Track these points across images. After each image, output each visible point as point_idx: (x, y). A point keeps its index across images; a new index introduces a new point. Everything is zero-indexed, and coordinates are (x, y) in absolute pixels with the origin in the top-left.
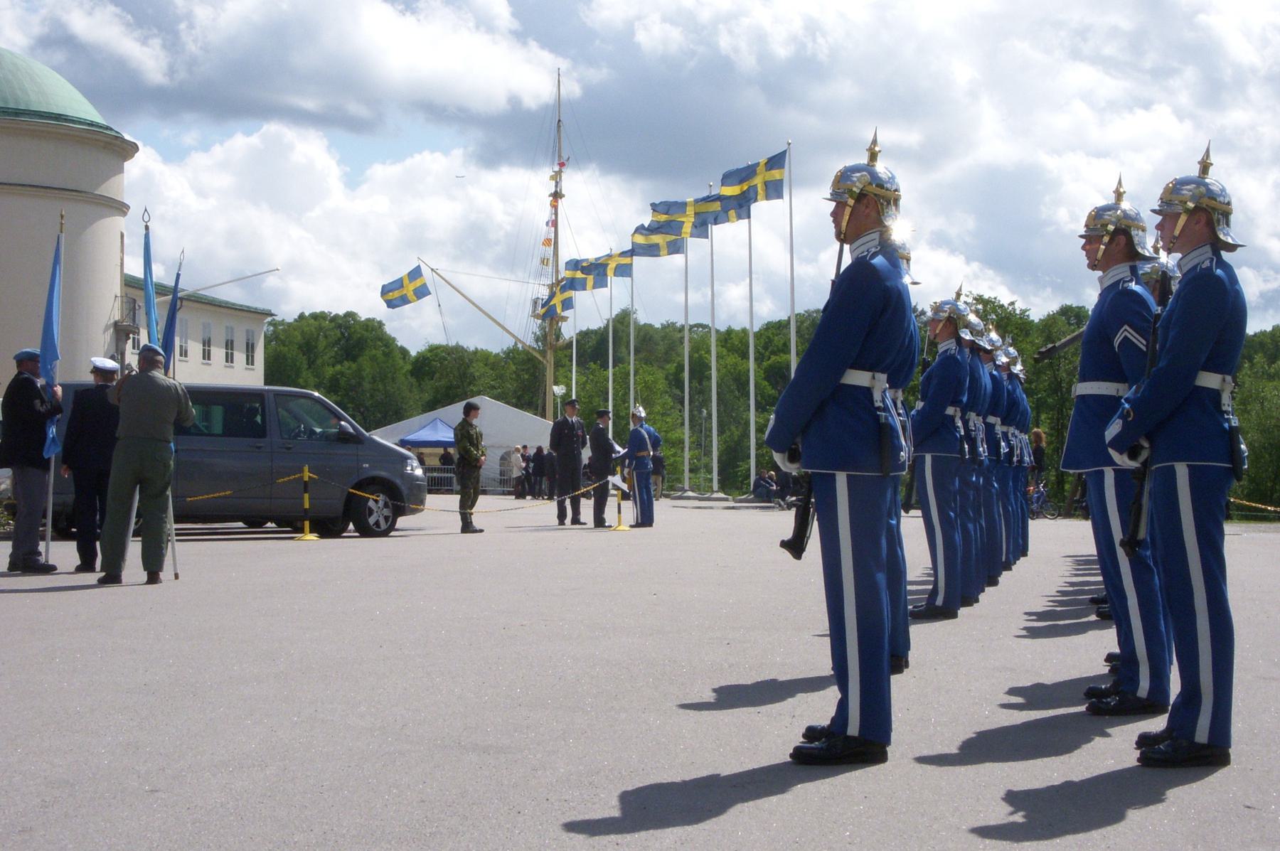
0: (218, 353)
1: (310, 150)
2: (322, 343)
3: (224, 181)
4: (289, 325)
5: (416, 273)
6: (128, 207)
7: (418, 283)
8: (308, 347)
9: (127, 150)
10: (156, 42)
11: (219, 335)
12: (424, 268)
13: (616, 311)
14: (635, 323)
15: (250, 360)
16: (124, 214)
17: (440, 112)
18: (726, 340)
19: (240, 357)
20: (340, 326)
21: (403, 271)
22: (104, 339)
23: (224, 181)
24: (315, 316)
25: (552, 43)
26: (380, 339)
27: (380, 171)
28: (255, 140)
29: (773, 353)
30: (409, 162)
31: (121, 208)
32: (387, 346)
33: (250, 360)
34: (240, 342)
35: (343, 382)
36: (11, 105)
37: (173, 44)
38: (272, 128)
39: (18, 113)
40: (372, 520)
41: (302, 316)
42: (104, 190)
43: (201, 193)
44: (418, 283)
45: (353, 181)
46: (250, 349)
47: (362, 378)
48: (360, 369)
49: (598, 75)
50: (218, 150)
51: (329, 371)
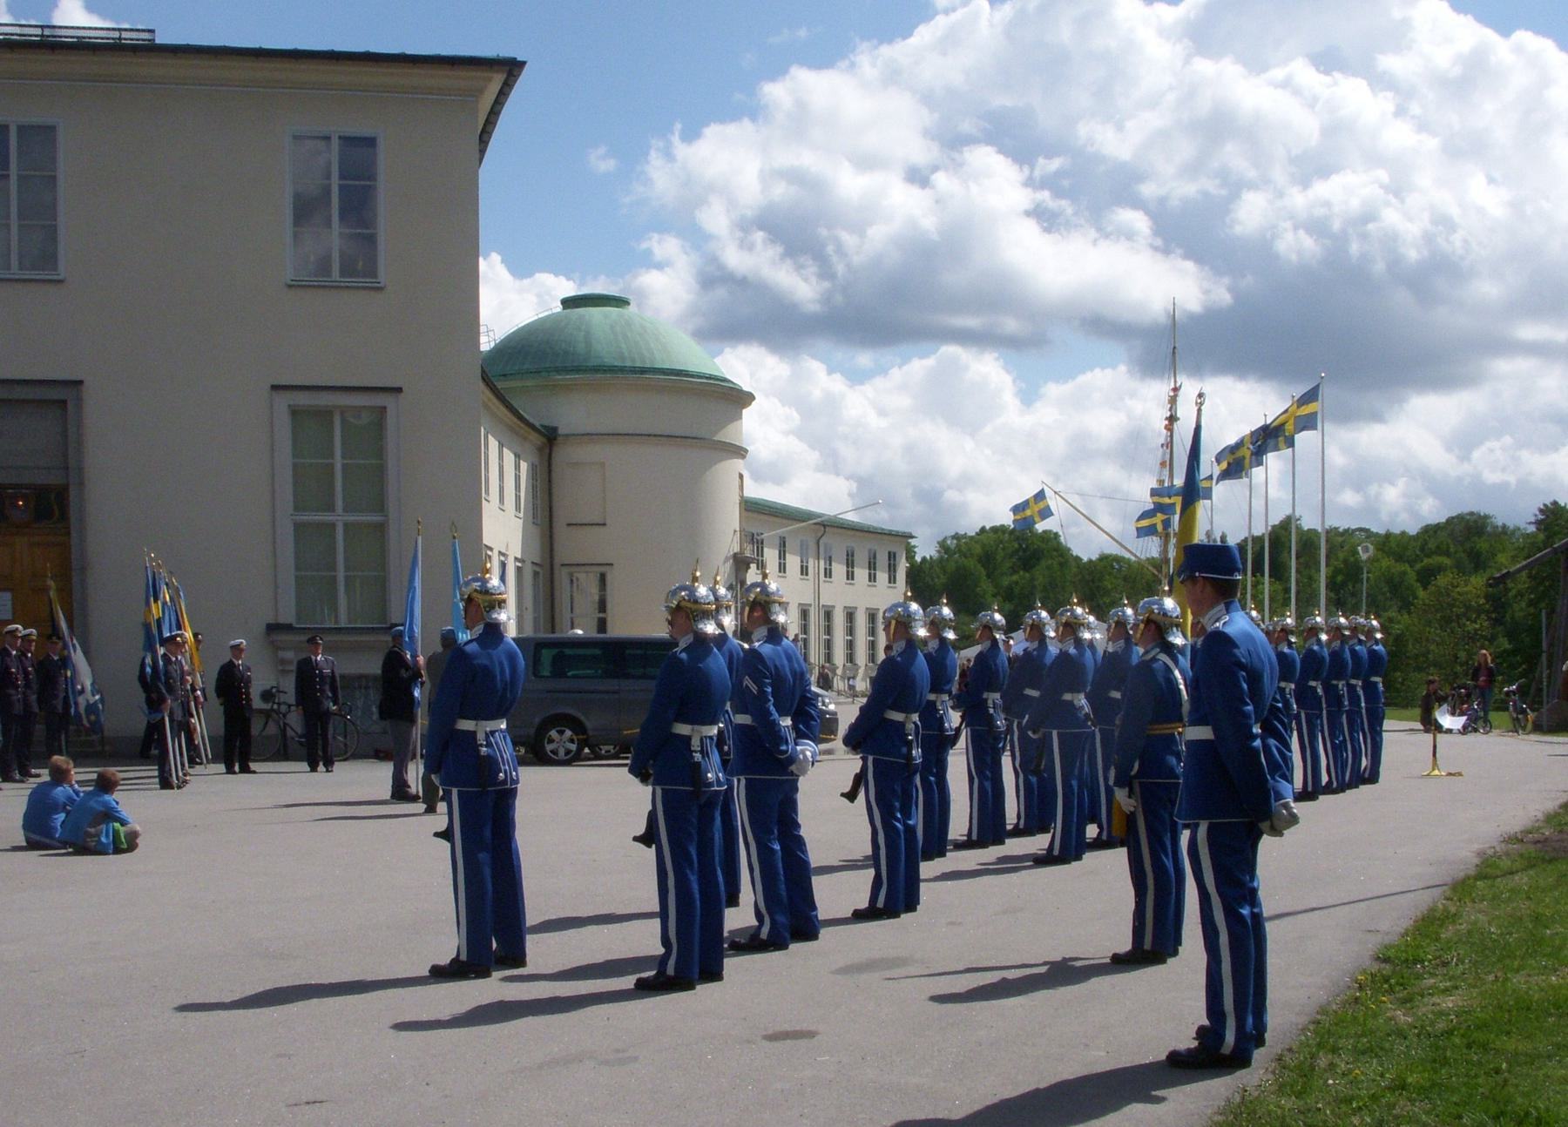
0: (861, 573)
1: (987, 370)
2: (1000, 555)
3: (904, 401)
4: (972, 538)
5: (1040, 496)
6: (746, 451)
7: (1041, 505)
8: (987, 559)
9: (738, 399)
10: (812, 269)
11: (861, 557)
12: (1047, 490)
13: (1276, 519)
14: (1299, 528)
15: (892, 579)
16: (743, 457)
17: (1105, 327)
18: (1384, 544)
19: (882, 576)
20: (1018, 538)
21: (1029, 493)
22: (725, 571)
23: (904, 401)
24: (995, 530)
25: (1196, 253)
26: (1056, 550)
27: (1053, 390)
28: (930, 362)
29: (1428, 556)
30: (1081, 379)
31: (740, 452)
32: (1061, 555)
33: (892, 579)
34: (882, 560)
35: (1016, 591)
36: (628, 364)
37: (826, 273)
38: (951, 350)
39: (643, 371)
40: (553, 733)
41: (983, 530)
42: (721, 437)
43: (882, 413)
44: (1041, 505)
45: (1028, 397)
46: (892, 569)
47: (1034, 587)
48: (1033, 579)
49: (1249, 279)
50: (896, 374)
51: (1006, 581)
